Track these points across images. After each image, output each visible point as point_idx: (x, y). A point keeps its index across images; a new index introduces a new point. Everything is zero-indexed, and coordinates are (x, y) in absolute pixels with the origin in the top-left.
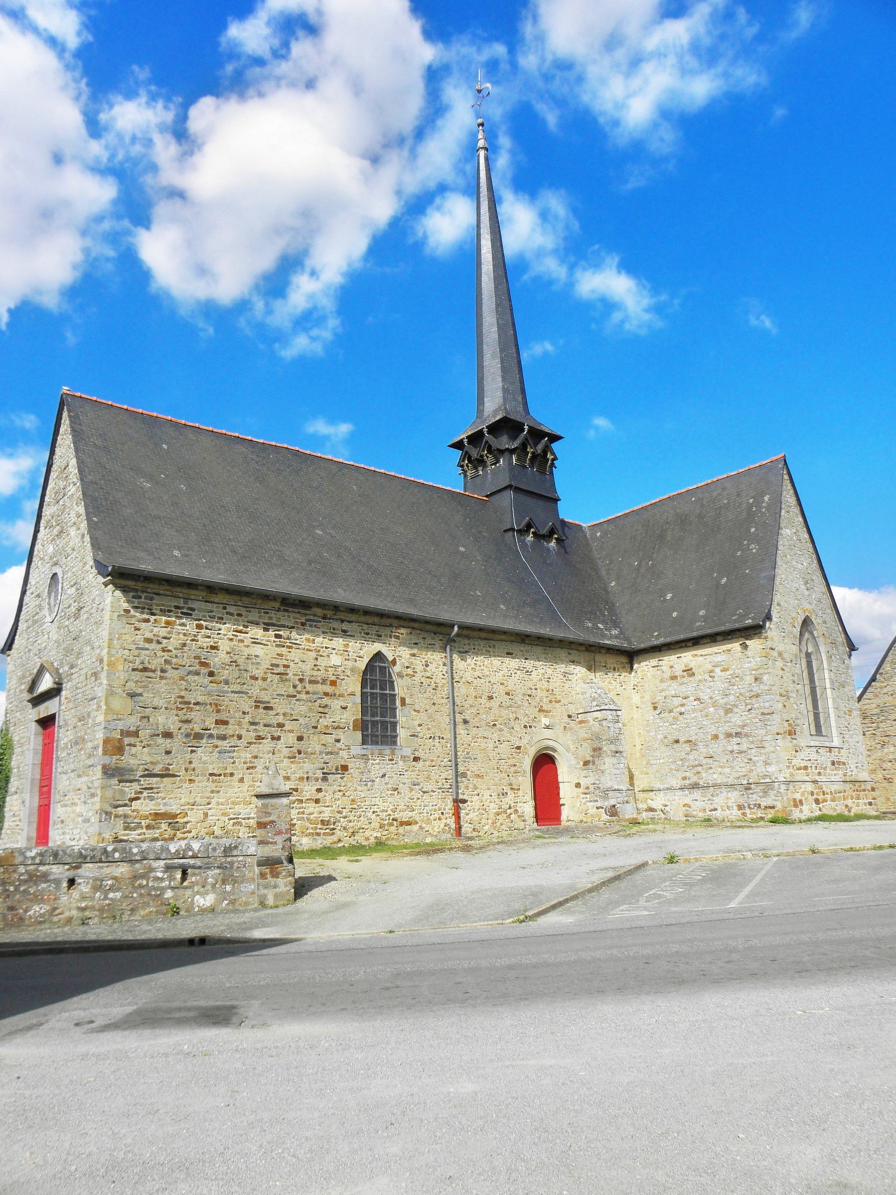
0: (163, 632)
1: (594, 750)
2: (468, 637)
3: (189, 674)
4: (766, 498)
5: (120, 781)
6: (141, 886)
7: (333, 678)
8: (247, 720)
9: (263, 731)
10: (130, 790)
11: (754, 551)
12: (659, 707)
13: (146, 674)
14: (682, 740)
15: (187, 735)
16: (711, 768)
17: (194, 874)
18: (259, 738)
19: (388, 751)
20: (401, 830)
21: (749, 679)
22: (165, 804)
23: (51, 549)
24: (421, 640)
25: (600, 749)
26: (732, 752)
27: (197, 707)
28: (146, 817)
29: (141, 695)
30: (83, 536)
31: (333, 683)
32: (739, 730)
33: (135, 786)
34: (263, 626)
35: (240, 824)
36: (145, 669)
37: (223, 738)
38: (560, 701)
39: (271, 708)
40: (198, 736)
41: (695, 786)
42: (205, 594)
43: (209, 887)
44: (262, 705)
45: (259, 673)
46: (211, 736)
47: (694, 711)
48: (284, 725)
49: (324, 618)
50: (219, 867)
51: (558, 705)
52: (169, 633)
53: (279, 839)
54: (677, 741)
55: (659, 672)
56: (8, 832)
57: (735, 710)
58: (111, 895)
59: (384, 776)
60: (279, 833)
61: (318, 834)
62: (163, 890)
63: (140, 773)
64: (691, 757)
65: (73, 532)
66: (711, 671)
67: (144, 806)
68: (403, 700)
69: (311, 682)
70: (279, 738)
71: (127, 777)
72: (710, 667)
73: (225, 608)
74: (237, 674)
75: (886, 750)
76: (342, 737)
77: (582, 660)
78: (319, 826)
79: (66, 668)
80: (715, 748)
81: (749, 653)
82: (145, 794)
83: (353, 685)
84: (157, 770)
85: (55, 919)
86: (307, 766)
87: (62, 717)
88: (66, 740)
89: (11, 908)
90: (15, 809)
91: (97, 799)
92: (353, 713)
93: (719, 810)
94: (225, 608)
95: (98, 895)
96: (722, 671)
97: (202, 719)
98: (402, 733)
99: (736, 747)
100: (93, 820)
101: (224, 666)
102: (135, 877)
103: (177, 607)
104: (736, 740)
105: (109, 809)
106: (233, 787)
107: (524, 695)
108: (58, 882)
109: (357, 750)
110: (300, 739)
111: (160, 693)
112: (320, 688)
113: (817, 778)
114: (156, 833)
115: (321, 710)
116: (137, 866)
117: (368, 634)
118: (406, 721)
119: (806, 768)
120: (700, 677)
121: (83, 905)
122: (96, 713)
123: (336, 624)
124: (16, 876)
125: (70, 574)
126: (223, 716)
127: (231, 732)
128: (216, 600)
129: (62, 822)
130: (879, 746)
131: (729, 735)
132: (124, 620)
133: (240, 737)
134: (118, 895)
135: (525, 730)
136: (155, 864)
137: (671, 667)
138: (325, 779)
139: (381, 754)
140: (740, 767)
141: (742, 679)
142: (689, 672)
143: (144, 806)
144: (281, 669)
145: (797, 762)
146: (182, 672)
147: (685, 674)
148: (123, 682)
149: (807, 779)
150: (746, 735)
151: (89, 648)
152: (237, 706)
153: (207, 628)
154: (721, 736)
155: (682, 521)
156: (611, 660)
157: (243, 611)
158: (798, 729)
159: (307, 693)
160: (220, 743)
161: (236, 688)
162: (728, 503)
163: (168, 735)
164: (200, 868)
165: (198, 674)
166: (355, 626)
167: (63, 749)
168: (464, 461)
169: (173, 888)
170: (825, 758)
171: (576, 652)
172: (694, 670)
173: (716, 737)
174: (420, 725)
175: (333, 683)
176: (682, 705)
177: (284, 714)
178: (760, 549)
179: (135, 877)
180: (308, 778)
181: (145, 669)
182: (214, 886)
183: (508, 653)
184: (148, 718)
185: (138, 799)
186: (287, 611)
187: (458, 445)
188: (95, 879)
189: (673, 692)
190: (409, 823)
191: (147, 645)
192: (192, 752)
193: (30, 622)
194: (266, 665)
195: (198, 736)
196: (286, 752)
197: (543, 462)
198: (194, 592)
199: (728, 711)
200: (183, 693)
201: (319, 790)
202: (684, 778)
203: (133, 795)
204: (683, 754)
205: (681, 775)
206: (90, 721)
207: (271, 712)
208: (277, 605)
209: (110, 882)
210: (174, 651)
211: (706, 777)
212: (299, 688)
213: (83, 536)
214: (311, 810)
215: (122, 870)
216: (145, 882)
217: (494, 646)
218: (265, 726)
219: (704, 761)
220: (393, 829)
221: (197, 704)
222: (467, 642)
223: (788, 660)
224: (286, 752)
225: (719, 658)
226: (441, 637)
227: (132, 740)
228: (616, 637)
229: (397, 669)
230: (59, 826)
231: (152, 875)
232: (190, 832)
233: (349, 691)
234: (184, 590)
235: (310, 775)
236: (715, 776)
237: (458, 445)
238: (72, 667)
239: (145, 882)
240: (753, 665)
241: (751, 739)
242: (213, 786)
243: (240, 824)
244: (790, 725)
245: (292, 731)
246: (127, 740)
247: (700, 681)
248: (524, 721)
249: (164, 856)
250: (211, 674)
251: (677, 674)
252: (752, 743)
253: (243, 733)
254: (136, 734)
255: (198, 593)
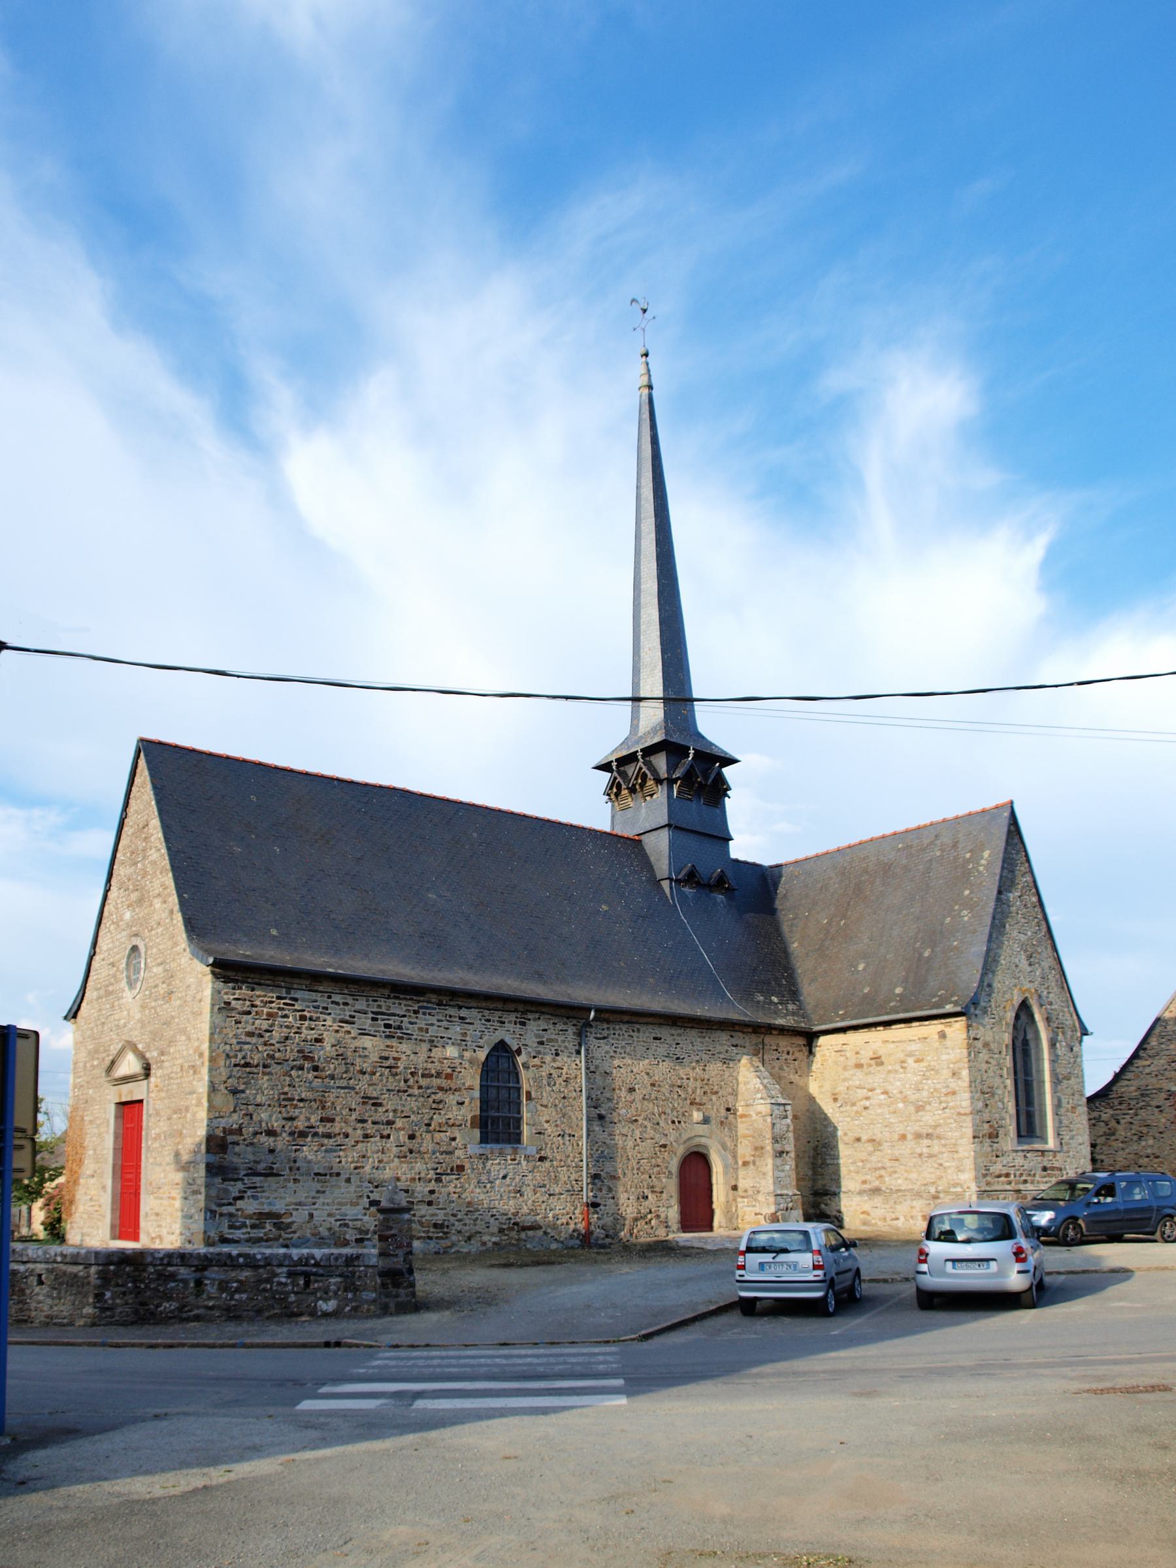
0: (265, 1025)
1: (756, 1149)
2: (608, 1022)
3: (292, 1069)
4: (986, 854)
5: (224, 1180)
6: (265, 1290)
7: (449, 1071)
8: (354, 1117)
9: (370, 1128)
10: (235, 1189)
11: (966, 919)
12: (840, 1098)
13: (248, 1069)
14: (864, 1138)
15: (292, 1134)
16: (895, 1172)
17: (317, 1281)
18: (366, 1136)
19: (508, 1148)
20: (523, 1235)
21: (946, 1073)
22: (270, 1204)
23: (128, 916)
24: (551, 1026)
25: (762, 1148)
26: (920, 1155)
27: (301, 1105)
28: (250, 1217)
29: (243, 1091)
30: (172, 912)
31: (449, 1077)
32: (930, 1131)
33: (239, 1185)
34: (371, 1015)
35: (346, 1225)
36: (247, 1065)
37: (328, 1136)
38: (716, 1093)
39: (380, 1105)
40: (303, 1134)
41: (876, 1191)
42: (308, 982)
43: (331, 1294)
44: (371, 1102)
45: (367, 1066)
46: (315, 1134)
47: (880, 1106)
48: (393, 1123)
49: (440, 1004)
50: (340, 1276)
51: (714, 1098)
52: (272, 1025)
53: (400, 1252)
54: (859, 1140)
55: (842, 1059)
56: (85, 1216)
57: (928, 1108)
58: (237, 1296)
59: (504, 1177)
60: (399, 1247)
61: (430, 1238)
62: (287, 1294)
63: (243, 1173)
64: (874, 1158)
65: (157, 904)
66: (903, 1062)
67: (249, 1206)
68: (529, 1093)
69: (423, 1076)
70: (388, 1136)
71: (231, 1176)
72: (901, 1056)
73: (329, 997)
74: (343, 1068)
75: (1143, 1143)
76: (458, 1135)
77: (747, 1044)
78: (432, 1230)
79: (155, 1054)
80: (904, 1149)
81: (948, 1043)
82: (249, 1193)
83: (471, 1078)
84: (261, 1167)
85: (184, 1315)
86: (419, 1166)
87: (151, 1106)
88: (157, 1131)
89: (143, 1304)
90: (93, 1193)
91: (202, 1197)
92: (471, 1109)
93: (902, 1219)
94: (329, 997)
95: (224, 1295)
96: (916, 1061)
97: (305, 1117)
98: (526, 1130)
99: (925, 1150)
100: (196, 1217)
101: (328, 1060)
102: (260, 1281)
103: (279, 998)
104: (926, 1142)
105: (214, 1207)
106: (340, 1187)
107: (673, 1086)
108: (185, 1282)
109: (474, 1149)
110: (412, 1137)
111: (264, 1088)
112: (436, 1082)
113: (1021, 1187)
114: (260, 1233)
115: (434, 1106)
116: (261, 1270)
117: (489, 1021)
118: (533, 1118)
119: (1007, 1175)
120: (890, 1068)
121: (211, 1304)
122: (195, 1109)
123: (452, 1011)
124: (145, 1274)
125: (154, 950)
126: (330, 1113)
127: (337, 1130)
128: (321, 988)
129: (157, 1214)
130: (1135, 1138)
131: (918, 1136)
132: (225, 1013)
133: (347, 1136)
134: (244, 1296)
135: (672, 1126)
136: (279, 1270)
137: (857, 1053)
138: (438, 1180)
139: (501, 1154)
140: (928, 1172)
141: (937, 1072)
142: (877, 1060)
143: (249, 1206)
144: (390, 1062)
145: (997, 1168)
146: (286, 1068)
147: (873, 1062)
148: (224, 1079)
149: (1008, 1187)
150: (939, 1137)
151: (183, 1038)
152: (341, 1101)
153: (311, 1019)
154: (909, 1137)
155: (886, 869)
156: (784, 1043)
157: (350, 1000)
158: (1001, 1131)
159: (420, 1087)
160: (326, 1141)
161: (343, 1083)
162: (942, 857)
163: (271, 1133)
164: (322, 1275)
165: (301, 1068)
166: (474, 1012)
167: (155, 1139)
168: (611, 788)
169: (296, 1293)
170: (1034, 1162)
171: (740, 1034)
172: (883, 1059)
173: (903, 1137)
174: (547, 1122)
175: (449, 1077)
176: (867, 1098)
177: (395, 1111)
178: (973, 917)
179: (260, 1281)
180: (420, 1179)
181: (247, 1065)
182: (336, 1293)
183: (655, 1038)
184: (251, 1115)
185: (241, 1198)
186: (398, 998)
187: (605, 767)
188: (221, 1282)
189: (857, 1083)
190: (531, 1228)
191: (248, 1039)
192: (296, 1151)
193: (102, 992)
194: (374, 1057)
195: (303, 1134)
196: (395, 1150)
197: (718, 790)
198: (297, 981)
199: (919, 1109)
200: (286, 1089)
201: (432, 1192)
202: (864, 1182)
203: (237, 1194)
204: (864, 1154)
205: (860, 1178)
206: (189, 1115)
207: (380, 1109)
208: (386, 992)
209: (235, 1285)
210: (277, 1045)
211: (889, 1182)
212: (411, 1082)
213: (172, 912)
214: (423, 1212)
215: (245, 1274)
216: (269, 1286)
217: (638, 1030)
218: (374, 1123)
219: (888, 1164)
220: (514, 1234)
221: (301, 1100)
222: (605, 1026)
223: (996, 1051)
224: (395, 1150)
225: (913, 1047)
226: (574, 1022)
227: (235, 1138)
228: (793, 1014)
229: (520, 1060)
230: (153, 1217)
231: (276, 1280)
232: (294, 1232)
233: (467, 1085)
234: (288, 979)
235: (422, 1175)
236: (899, 1181)
237: (605, 767)
238: (162, 1054)
239: (269, 1286)
240: (952, 1057)
241: (943, 1142)
242: (318, 1186)
243: (346, 1225)
244: (991, 1127)
245: (403, 1129)
246: (230, 1138)
247: (889, 1072)
248: (673, 1116)
249: (287, 1263)
250: (316, 1069)
251: (862, 1061)
252: (945, 1146)
253: (350, 1131)
254: (239, 1131)
255: (302, 981)
